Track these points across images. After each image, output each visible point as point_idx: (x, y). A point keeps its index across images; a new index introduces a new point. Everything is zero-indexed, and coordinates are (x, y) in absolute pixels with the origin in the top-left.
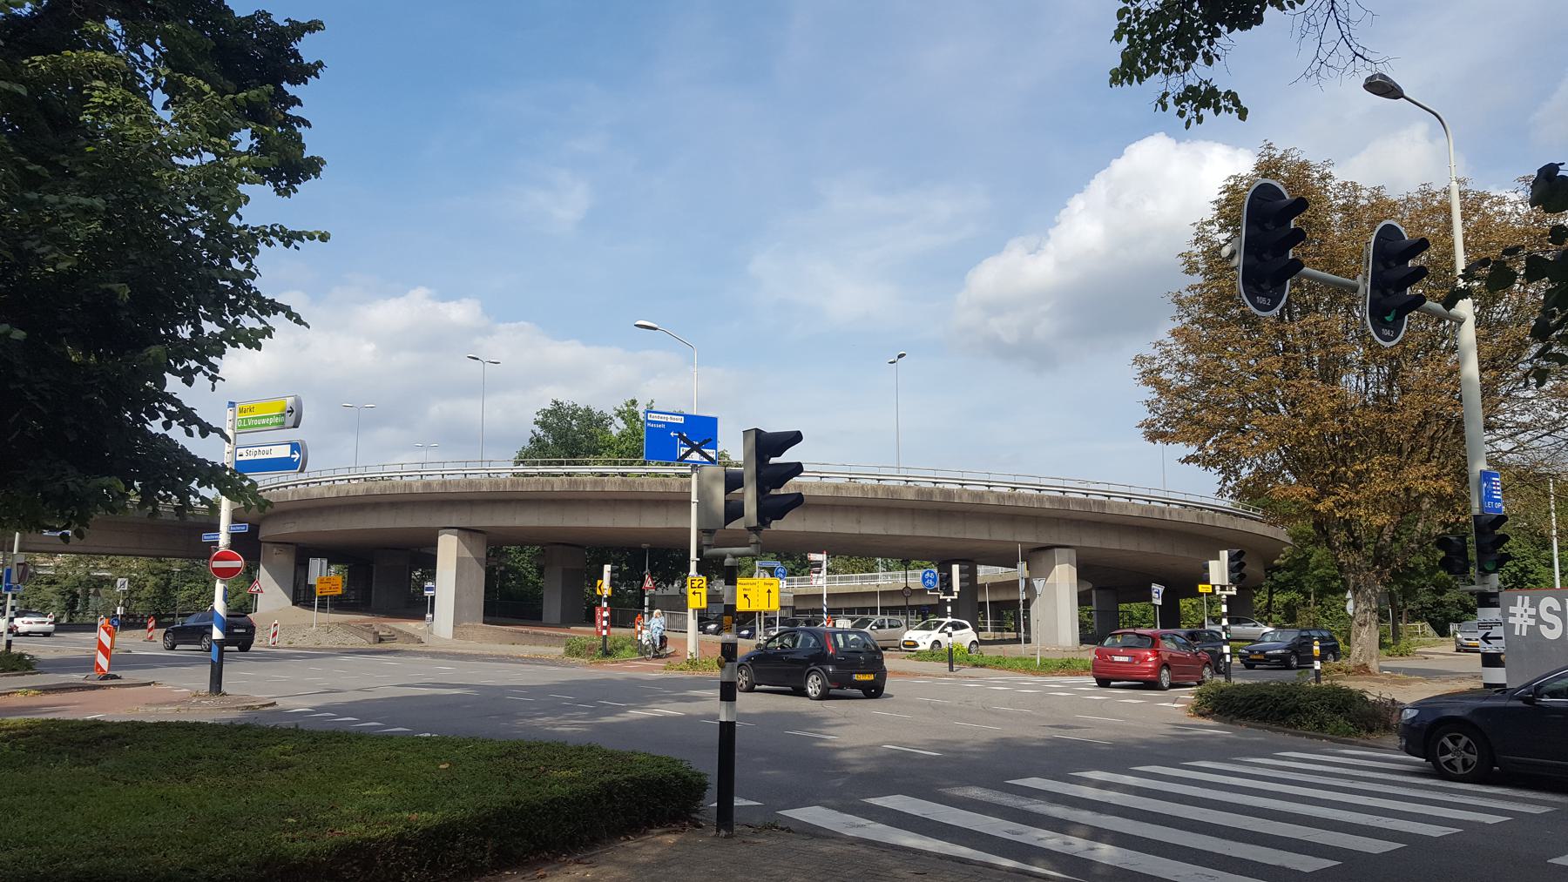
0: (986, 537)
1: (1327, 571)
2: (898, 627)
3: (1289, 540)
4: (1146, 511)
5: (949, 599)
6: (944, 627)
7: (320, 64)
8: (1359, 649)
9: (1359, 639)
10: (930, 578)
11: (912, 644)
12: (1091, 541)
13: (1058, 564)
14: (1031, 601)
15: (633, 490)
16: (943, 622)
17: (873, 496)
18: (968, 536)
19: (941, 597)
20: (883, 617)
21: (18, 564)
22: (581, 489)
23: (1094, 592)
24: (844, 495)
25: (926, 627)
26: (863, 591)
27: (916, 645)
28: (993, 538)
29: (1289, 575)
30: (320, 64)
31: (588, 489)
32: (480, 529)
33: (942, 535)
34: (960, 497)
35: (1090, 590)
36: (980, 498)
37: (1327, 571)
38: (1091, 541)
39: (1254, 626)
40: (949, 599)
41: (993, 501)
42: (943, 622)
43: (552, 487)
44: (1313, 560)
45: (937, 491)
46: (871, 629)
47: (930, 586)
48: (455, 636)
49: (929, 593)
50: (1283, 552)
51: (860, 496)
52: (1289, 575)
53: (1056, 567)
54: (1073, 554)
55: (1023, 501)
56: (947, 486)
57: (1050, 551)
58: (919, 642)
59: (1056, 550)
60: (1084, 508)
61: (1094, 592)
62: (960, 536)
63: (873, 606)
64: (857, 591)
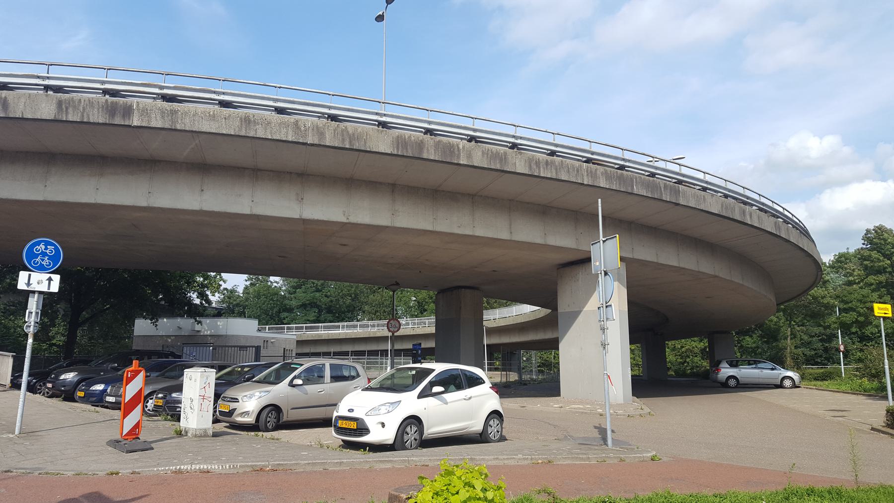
2: (353, 378)
4: (726, 208)
6: (432, 384)
7: (595, 427)
11: (353, 425)
16: (430, 371)
17: (316, 142)
18: (479, 232)
21: (358, 376)
24: (261, 134)
25: (391, 386)
26: (377, 336)
27: (363, 430)
29: (224, 468)
30: (595, 427)
33: (439, 228)
36: (501, 160)
42: (434, 370)
46: (291, 384)
51: (290, 139)
52: (224, 468)
55: (568, 172)
58: (370, 423)
62: (468, 232)
63: (386, 349)
64: (372, 335)
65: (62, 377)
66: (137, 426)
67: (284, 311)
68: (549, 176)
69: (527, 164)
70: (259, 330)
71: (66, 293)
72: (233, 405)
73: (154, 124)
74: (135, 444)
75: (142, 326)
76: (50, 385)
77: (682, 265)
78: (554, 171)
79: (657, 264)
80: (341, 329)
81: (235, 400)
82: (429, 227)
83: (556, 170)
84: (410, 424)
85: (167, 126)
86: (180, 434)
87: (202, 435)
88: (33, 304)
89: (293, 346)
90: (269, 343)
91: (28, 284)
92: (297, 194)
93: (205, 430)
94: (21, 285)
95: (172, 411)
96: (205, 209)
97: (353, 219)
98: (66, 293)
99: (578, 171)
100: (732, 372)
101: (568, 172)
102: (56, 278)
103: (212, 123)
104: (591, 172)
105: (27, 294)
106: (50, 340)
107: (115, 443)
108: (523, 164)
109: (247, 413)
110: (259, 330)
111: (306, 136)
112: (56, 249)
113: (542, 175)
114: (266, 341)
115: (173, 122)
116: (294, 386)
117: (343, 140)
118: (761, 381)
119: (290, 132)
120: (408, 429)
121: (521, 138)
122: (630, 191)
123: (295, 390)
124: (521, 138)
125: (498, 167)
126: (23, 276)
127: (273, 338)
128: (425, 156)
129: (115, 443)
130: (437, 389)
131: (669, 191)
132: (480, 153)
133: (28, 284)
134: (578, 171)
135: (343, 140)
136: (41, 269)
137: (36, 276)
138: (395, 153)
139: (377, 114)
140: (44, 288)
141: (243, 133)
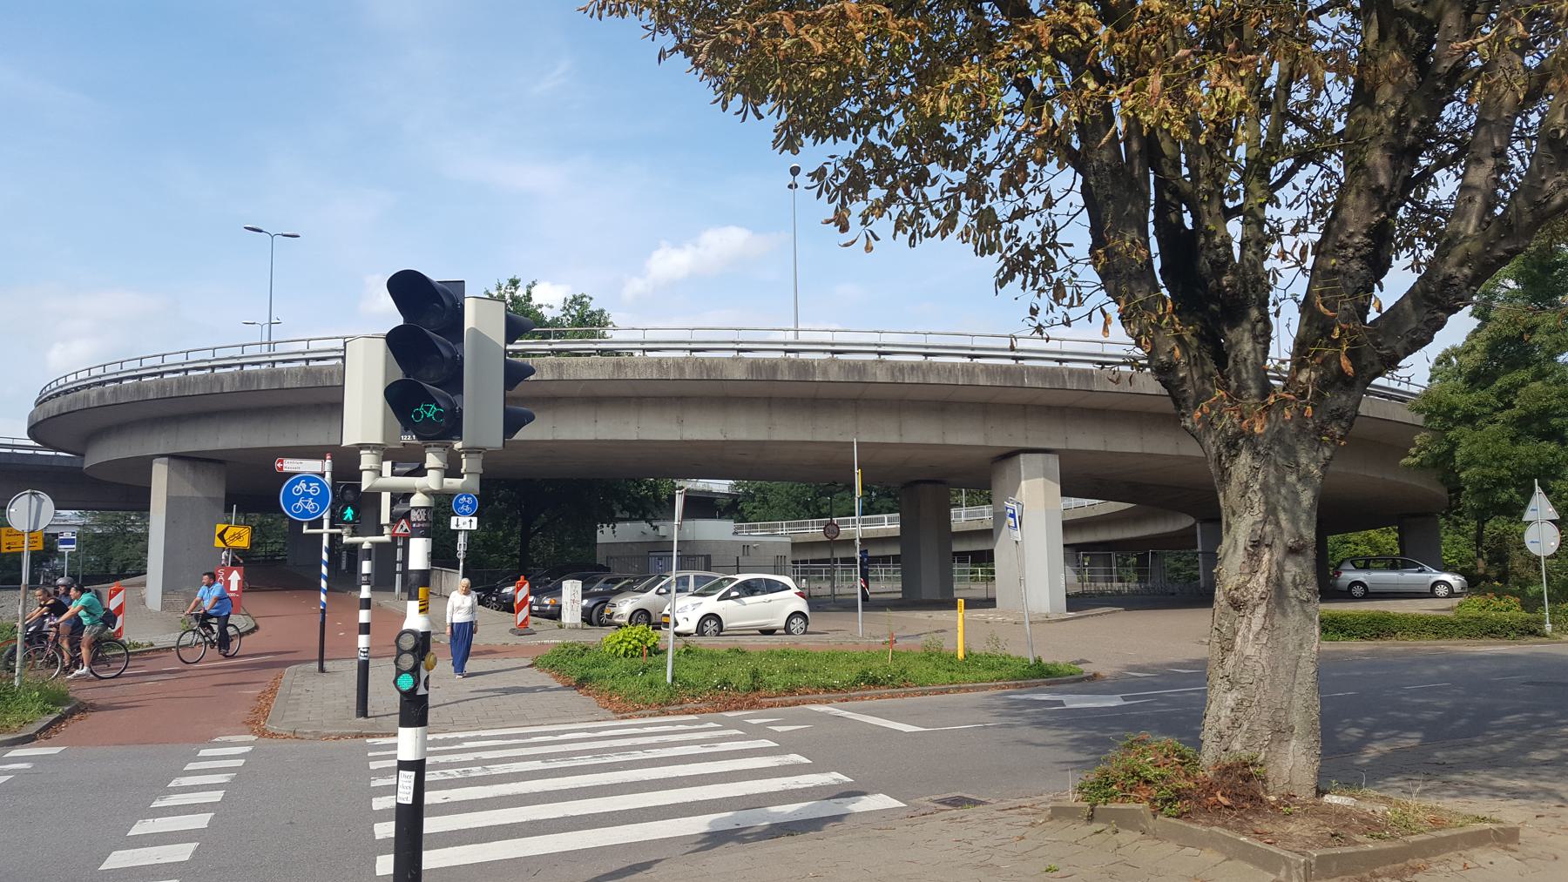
0: (893, 438)
1: (1486, 471)
3: (1420, 420)
5: (366, 542)
6: (734, 589)
8: (1231, 699)
9: (1231, 660)
10: (466, 504)
12: (1087, 440)
13: (1026, 479)
14: (995, 532)
15: (320, 384)
19: (346, 539)
20: (683, 573)
22: (255, 388)
23: (1198, 526)
24: (630, 376)
28: (906, 440)
31: (263, 387)
32: (207, 456)
34: (825, 372)
35: (1194, 526)
36: (859, 372)
37: (1486, 471)
38: (1087, 440)
39: (1420, 571)
40: (366, 542)
41: (882, 377)
43: (222, 387)
44: (1460, 454)
45: (786, 364)
47: (305, 513)
48: (164, 607)
49: (305, 530)
50: (1414, 445)
51: (655, 377)
53: (1023, 483)
54: (1054, 462)
55: (938, 374)
56: (802, 356)
57: (1014, 459)
59: (1022, 457)
60: (1050, 382)
61: (1198, 526)
65: (504, 591)
66: (526, 619)
67: (821, 495)
68: (915, 381)
69: (889, 373)
70: (735, 533)
71: (850, 190)
72: (612, 610)
73: (545, 377)
74: (527, 631)
75: (605, 535)
76: (494, 599)
77: (1147, 450)
78: (920, 375)
79: (1105, 452)
80: (886, 523)
81: (614, 605)
82: (809, 438)
83: (923, 374)
84: (710, 619)
85: (556, 378)
86: (561, 627)
87: (576, 627)
88: (461, 539)
89: (787, 552)
90: (751, 549)
91: (457, 525)
92: (678, 417)
93: (576, 625)
94: (453, 527)
95: (555, 615)
96: (599, 438)
97: (730, 437)
98: (850, 190)
99: (950, 371)
100: (1361, 576)
101: (938, 374)
102: (475, 519)
103: (591, 371)
104: (967, 371)
105: (456, 532)
106: (511, 551)
107: (512, 631)
108: (884, 371)
109: (621, 616)
110: (735, 533)
111: (668, 372)
112: (473, 499)
113: (907, 381)
114: (746, 547)
115: (561, 374)
116: (660, 594)
117: (701, 372)
118: (1402, 588)
119: (655, 371)
120: (708, 623)
121: (884, 345)
122: (1019, 384)
123: (661, 598)
124: (884, 345)
125: (856, 379)
126: (454, 519)
127: (756, 542)
128: (779, 377)
129: (512, 631)
130: (734, 594)
131: (1076, 377)
132: (836, 368)
133: (457, 525)
134: (950, 371)
135: (701, 372)
136: (465, 514)
137: (462, 519)
138: (750, 378)
139: (733, 342)
140: (467, 527)
141: (615, 377)
